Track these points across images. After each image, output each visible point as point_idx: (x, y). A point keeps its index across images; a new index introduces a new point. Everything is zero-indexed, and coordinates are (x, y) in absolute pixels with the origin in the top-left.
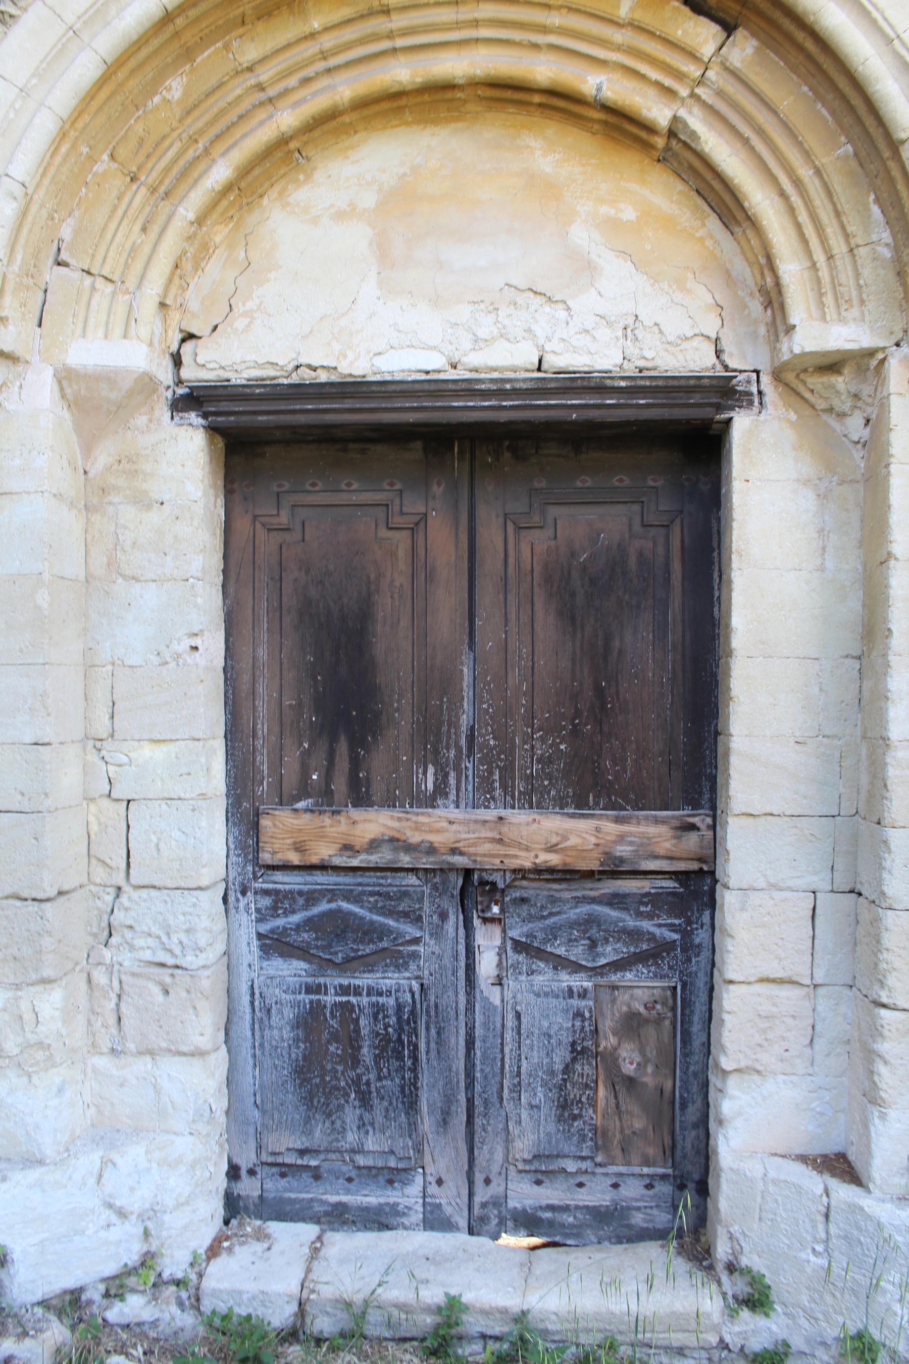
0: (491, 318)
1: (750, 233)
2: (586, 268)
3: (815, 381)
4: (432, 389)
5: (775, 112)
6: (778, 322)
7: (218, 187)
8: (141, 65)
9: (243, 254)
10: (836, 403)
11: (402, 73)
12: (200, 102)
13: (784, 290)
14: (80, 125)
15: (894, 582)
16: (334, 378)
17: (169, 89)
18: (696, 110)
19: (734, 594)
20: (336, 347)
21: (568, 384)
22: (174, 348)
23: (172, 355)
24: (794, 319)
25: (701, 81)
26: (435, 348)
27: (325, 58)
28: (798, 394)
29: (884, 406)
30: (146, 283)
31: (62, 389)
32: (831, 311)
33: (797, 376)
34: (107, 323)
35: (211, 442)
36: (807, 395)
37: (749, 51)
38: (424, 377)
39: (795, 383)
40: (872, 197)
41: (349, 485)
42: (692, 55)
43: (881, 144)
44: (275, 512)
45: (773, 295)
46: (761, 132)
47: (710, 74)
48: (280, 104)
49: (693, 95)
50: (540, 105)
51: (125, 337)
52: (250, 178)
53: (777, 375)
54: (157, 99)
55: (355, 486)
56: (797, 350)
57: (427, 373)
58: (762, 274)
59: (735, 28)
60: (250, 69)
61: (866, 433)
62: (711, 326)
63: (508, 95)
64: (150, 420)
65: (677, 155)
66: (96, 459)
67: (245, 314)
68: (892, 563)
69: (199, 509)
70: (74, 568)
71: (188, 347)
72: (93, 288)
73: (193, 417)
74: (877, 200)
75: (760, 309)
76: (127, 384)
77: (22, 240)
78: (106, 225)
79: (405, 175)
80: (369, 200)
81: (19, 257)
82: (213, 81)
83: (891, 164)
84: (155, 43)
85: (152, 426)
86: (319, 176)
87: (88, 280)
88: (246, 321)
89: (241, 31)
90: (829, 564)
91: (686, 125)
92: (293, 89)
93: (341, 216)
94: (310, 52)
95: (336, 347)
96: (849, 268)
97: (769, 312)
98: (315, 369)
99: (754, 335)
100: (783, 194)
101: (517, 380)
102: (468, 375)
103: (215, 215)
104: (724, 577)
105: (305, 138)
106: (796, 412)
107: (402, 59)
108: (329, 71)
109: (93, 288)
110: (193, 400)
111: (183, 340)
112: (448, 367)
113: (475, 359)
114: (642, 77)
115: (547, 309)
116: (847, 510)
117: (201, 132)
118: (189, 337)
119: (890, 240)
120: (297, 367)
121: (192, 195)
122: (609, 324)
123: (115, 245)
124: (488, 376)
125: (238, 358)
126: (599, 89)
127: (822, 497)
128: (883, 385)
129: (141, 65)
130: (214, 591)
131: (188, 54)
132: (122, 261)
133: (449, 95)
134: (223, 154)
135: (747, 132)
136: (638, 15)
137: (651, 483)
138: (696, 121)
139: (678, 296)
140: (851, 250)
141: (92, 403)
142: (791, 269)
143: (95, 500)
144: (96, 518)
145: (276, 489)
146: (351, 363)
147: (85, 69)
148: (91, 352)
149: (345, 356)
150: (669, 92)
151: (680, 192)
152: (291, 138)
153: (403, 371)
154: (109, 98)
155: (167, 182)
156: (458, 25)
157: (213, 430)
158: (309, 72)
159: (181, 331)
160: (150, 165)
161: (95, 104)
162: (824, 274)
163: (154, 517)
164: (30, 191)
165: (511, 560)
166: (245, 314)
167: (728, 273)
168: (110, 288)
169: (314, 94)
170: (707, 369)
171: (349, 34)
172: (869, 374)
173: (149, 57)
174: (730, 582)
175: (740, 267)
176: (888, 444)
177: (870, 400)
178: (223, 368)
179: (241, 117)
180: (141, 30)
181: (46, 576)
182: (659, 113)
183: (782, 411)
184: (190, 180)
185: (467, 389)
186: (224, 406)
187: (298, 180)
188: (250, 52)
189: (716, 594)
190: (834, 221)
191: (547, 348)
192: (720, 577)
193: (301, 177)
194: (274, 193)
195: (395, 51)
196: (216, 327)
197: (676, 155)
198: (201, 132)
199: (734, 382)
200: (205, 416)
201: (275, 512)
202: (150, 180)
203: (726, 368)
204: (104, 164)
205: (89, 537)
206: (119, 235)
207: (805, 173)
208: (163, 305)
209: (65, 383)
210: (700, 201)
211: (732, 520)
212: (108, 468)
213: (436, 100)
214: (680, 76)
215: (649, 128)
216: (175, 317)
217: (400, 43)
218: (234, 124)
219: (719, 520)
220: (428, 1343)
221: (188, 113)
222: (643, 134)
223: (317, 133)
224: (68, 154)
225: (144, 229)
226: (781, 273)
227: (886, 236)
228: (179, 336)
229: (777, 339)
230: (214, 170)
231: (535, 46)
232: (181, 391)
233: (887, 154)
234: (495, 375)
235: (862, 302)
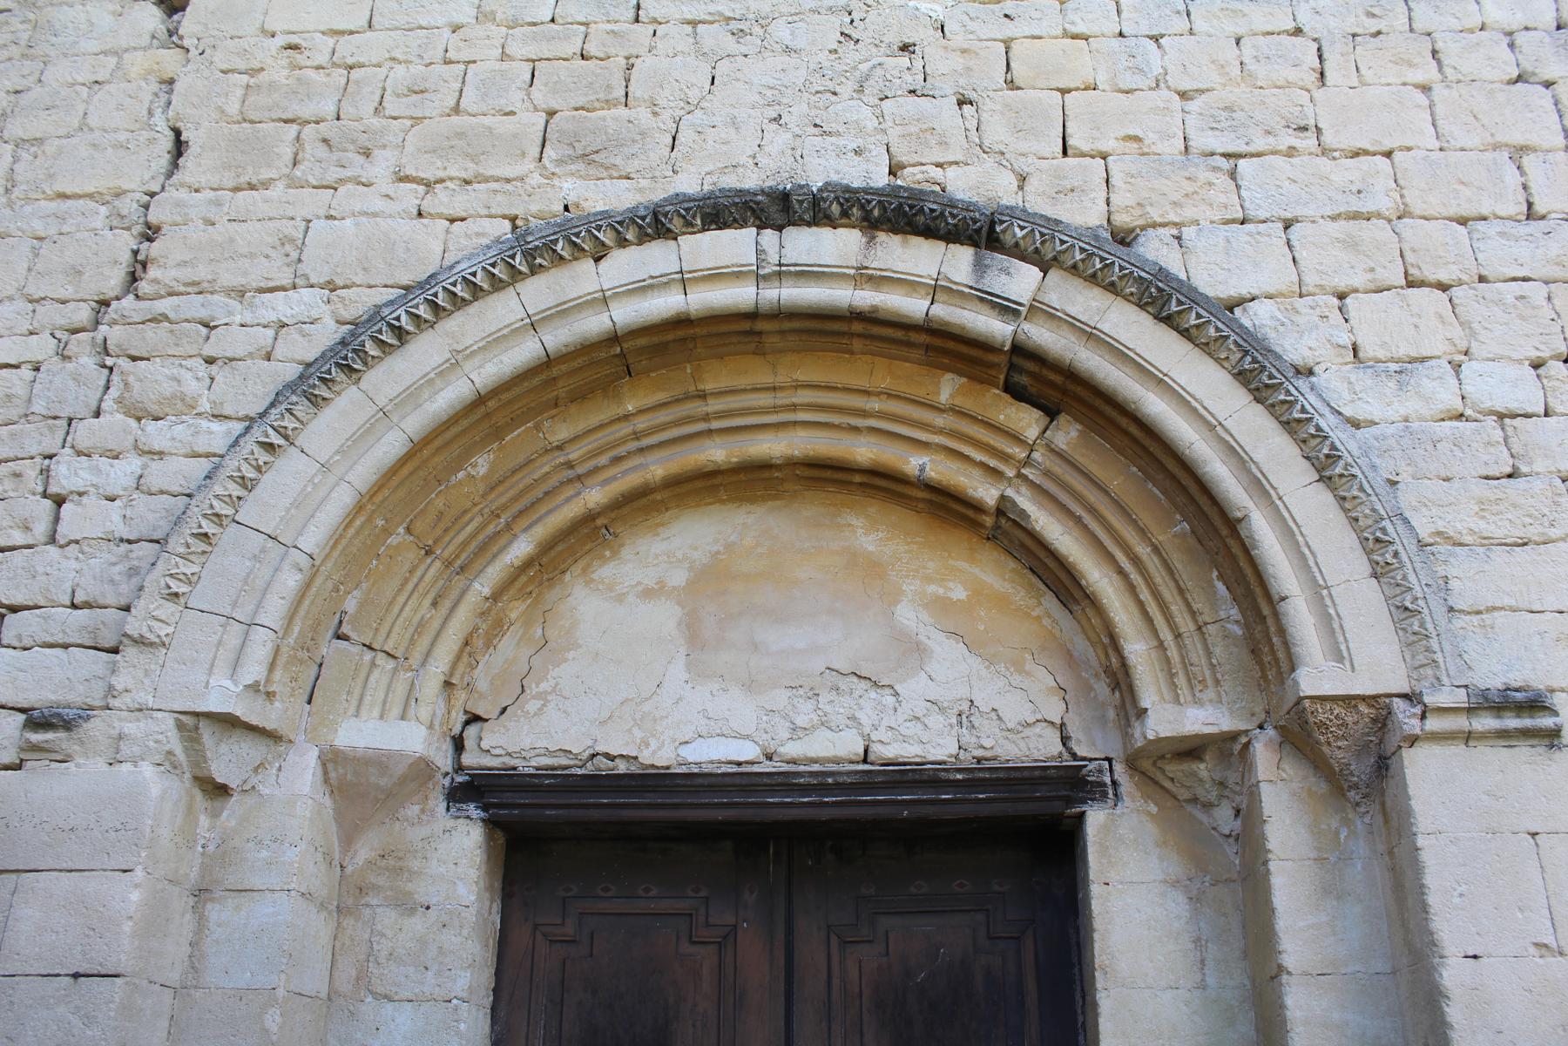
0: (810, 705)
1: (1090, 612)
2: (916, 652)
3: (1173, 768)
4: (739, 782)
5: (1107, 493)
6: (1129, 709)
7: (517, 563)
8: (448, 444)
9: (540, 631)
10: (1200, 792)
11: (717, 453)
12: (506, 478)
13: (1132, 671)
14: (379, 498)
15: (1289, 1001)
16: (634, 769)
17: (474, 466)
18: (1023, 489)
19: (1101, 1020)
20: (638, 734)
21: (898, 777)
22: (457, 730)
23: (453, 738)
24: (1145, 703)
25: (1028, 462)
26: (747, 737)
27: (638, 439)
28: (1156, 783)
29: (1254, 794)
30: (431, 660)
31: (326, 773)
32: (1184, 692)
33: (1154, 764)
34: (385, 702)
35: (490, 838)
36: (1167, 784)
37: (1074, 434)
38: (735, 769)
39: (1152, 771)
40: (1215, 573)
41: (647, 890)
42: (1017, 438)
43: (1218, 522)
44: (559, 921)
45: (1120, 676)
46: (1092, 510)
47: (1036, 455)
48: (589, 482)
49: (1019, 475)
50: (861, 484)
51: (403, 718)
52: (553, 553)
53: (1132, 763)
54: (461, 475)
55: (654, 892)
56: (1151, 736)
57: (739, 764)
58: (1107, 654)
59: (1058, 413)
60: (559, 448)
61: (1237, 825)
62: (1055, 711)
63: (826, 476)
64: (423, 811)
65: (1005, 533)
66: (356, 852)
67: (538, 696)
68: (1285, 977)
69: (470, 916)
70: (315, 982)
71: (472, 730)
72: (373, 664)
73: (473, 810)
74: (1221, 577)
75: (1108, 690)
76: (400, 770)
77: (302, 613)
78: (394, 598)
79: (718, 553)
80: (679, 578)
81: (296, 629)
82: (521, 459)
83: (1231, 542)
84: (465, 423)
85: (424, 817)
86: (626, 552)
87: (368, 655)
88: (539, 703)
89: (554, 412)
90: (1210, 981)
91: (1014, 503)
92: (604, 467)
93: (648, 594)
94: (623, 432)
95: (638, 734)
96: (1199, 646)
97: (1117, 694)
98: (612, 758)
99: (1102, 720)
100: (1121, 572)
101: (840, 773)
102: (786, 768)
103: (512, 592)
104: (1088, 998)
105: (613, 515)
106: (1156, 804)
107: (718, 440)
108: (641, 450)
109: (373, 664)
110: (475, 790)
111: (467, 723)
112: (762, 758)
113: (793, 749)
114: (966, 458)
115: (873, 695)
116: (1225, 915)
117: (504, 507)
118: (473, 719)
119: (1239, 617)
120: (594, 756)
121: (490, 570)
122: (942, 710)
123: (401, 619)
124: (808, 769)
125: (527, 744)
126: (922, 469)
127: (1195, 900)
128: (1250, 771)
129: (448, 444)
130: (481, 1015)
131: (497, 434)
132: (408, 636)
133: (766, 474)
134: (525, 530)
135: (1079, 511)
136: (958, 401)
137: (997, 888)
138: (1024, 501)
139: (1017, 679)
140: (1200, 628)
141: (359, 789)
142: (1137, 649)
143: (350, 902)
144: (348, 922)
145: (563, 894)
146: (654, 752)
147: (391, 446)
148: (360, 733)
149: (647, 745)
150: (996, 473)
151: (1013, 570)
152: (599, 514)
153: (712, 762)
154: (411, 474)
155: (463, 556)
156: (776, 409)
157: (491, 824)
158: (622, 451)
159: (466, 712)
160: (447, 539)
161: (396, 480)
162: (1173, 653)
163: (417, 924)
164: (317, 563)
165: (836, 981)
166: (538, 696)
167: (1069, 653)
168: (391, 664)
169: (625, 473)
170: (1053, 758)
171: (663, 417)
172: (1233, 759)
173: (457, 436)
174: (1095, 1005)
175: (1081, 646)
176: (1263, 838)
177: (1238, 788)
178: (509, 754)
179: (547, 493)
180: (451, 412)
181: (281, 992)
182: (987, 493)
183: (1140, 803)
184: (489, 555)
185: (783, 782)
186: (508, 798)
187: (603, 556)
188: (562, 432)
189: (1081, 1019)
190: (1178, 598)
191: (873, 738)
192: (1084, 998)
193: (608, 553)
194: (577, 569)
195: (710, 432)
196: (505, 709)
197: (1006, 533)
198: (504, 507)
199: (1084, 771)
200: (485, 808)
201: (559, 921)
202: (446, 554)
203: (1074, 756)
204: (399, 536)
205: (338, 944)
206: (407, 609)
207: (1143, 550)
208: (448, 684)
209: (330, 766)
210: (1035, 580)
211: (1093, 930)
212: (369, 862)
213: (751, 481)
214: (1005, 457)
215: (977, 507)
216: (460, 696)
217: (715, 425)
218: (539, 500)
219: (1077, 929)
220: (962, 755)
221: (492, 489)
222: (970, 513)
223: (625, 510)
224: (362, 527)
225: (435, 604)
226: (1126, 653)
227: (1235, 612)
228: (462, 718)
229: (1129, 725)
230: (515, 545)
231: (856, 429)
232: (460, 779)
233: (1225, 532)
234: (816, 768)
235: (1217, 682)
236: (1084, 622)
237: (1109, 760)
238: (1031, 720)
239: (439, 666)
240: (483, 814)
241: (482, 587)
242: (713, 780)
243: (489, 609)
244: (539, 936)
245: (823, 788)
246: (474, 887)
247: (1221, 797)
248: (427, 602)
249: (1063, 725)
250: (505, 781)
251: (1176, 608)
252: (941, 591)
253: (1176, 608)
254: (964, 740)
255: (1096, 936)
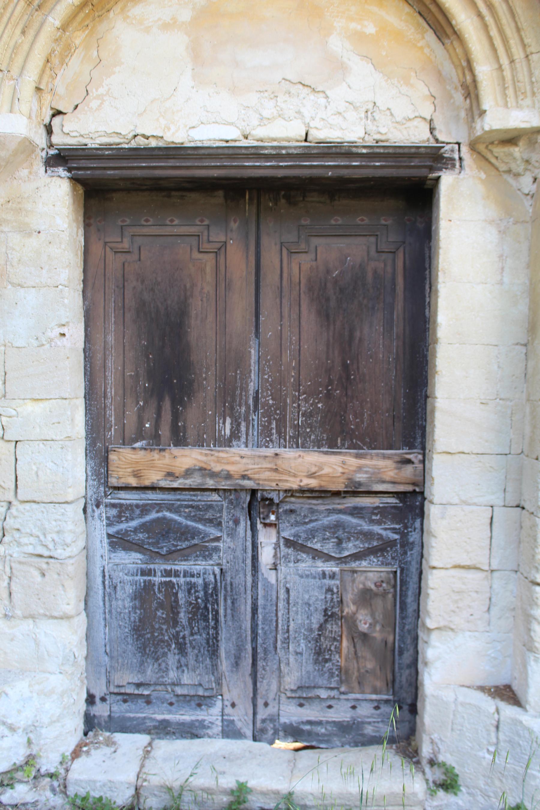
0: (272, 103)
1: (456, 44)
2: (340, 68)
3: (499, 151)
6: (475, 110)
9: (95, 53)
10: (513, 166)
13: (479, 85)
16: (161, 144)
21: (326, 151)
22: (47, 121)
23: (45, 126)
24: (485, 106)
28: (487, 160)
30: (25, 72)
32: (511, 100)
33: (487, 147)
35: (74, 189)
36: (493, 160)
38: (224, 144)
41: (172, 221)
44: (120, 240)
45: (471, 88)
51: (11, 112)
53: (473, 146)
55: (176, 222)
56: (487, 128)
57: (227, 141)
64: (30, 173)
71: (57, 121)
73: (61, 171)
75: (462, 98)
85: (32, 177)
90: (506, 280)
93: (166, 27)
96: (525, 69)
97: (468, 101)
98: (147, 138)
99: (457, 118)
101: (290, 147)
102: (256, 144)
103: (75, 24)
104: (433, 288)
106: (485, 173)
110: (60, 158)
111: (54, 116)
112: (241, 138)
115: (312, 97)
118: (58, 113)
121: (58, 7)
122: (356, 108)
124: (270, 144)
127: (502, 233)
132: (8, 55)
137: (383, 222)
140: (527, 56)
142: (484, 70)
145: (121, 224)
149: (169, 129)
153: (210, 140)
157: (75, 180)
159: (52, 109)
162: (507, 73)
165: (285, 275)
167: (439, 73)
170: (424, 142)
174: (437, 291)
175: (449, 69)
178: (82, 136)
185: (255, 153)
186: (83, 163)
189: (427, 300)
190: (516, 35)
191: (312, 125)
192: (430, 288)
194: (117, 9)
196: (76, 107)
199: (442, 150)
200: (69, 170)
201: (120, 240)
203: (437, 141)
208: (38, 89)
210: (421, 20)
211: (439, 248)
216: (47, 98)
219: (430, 248)
220: (367, 138)
225: (23, 32)
228: (51, 112)
229: (473, 120)
234: (275, 144)
235: (534, 94)
236: (451, 51)
237: (459, 144)
238: (412, 116)
239: (31, 77)
240: (68, 174)
241: (55, 19)
242: (211, 151)
243: (61, 38)
244: (108, 249)
245: (278, 157)
246: (66, 219)
247: (526, 170)
248: (18, 31)
249: (431, 120)
250: (80, 153)
251: (514, 42)
252: (359, 27)
253: (514, 42)
254: (368, 128)
255: (441, 251)
